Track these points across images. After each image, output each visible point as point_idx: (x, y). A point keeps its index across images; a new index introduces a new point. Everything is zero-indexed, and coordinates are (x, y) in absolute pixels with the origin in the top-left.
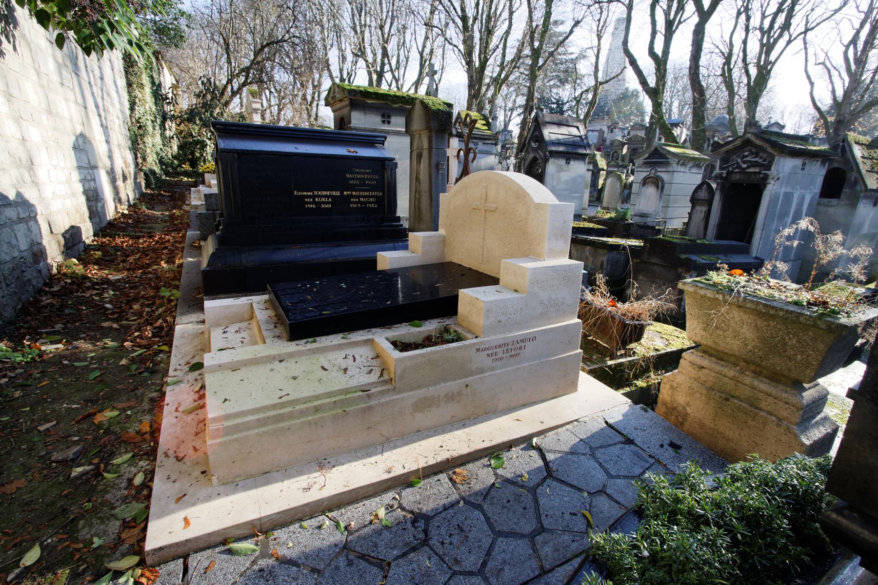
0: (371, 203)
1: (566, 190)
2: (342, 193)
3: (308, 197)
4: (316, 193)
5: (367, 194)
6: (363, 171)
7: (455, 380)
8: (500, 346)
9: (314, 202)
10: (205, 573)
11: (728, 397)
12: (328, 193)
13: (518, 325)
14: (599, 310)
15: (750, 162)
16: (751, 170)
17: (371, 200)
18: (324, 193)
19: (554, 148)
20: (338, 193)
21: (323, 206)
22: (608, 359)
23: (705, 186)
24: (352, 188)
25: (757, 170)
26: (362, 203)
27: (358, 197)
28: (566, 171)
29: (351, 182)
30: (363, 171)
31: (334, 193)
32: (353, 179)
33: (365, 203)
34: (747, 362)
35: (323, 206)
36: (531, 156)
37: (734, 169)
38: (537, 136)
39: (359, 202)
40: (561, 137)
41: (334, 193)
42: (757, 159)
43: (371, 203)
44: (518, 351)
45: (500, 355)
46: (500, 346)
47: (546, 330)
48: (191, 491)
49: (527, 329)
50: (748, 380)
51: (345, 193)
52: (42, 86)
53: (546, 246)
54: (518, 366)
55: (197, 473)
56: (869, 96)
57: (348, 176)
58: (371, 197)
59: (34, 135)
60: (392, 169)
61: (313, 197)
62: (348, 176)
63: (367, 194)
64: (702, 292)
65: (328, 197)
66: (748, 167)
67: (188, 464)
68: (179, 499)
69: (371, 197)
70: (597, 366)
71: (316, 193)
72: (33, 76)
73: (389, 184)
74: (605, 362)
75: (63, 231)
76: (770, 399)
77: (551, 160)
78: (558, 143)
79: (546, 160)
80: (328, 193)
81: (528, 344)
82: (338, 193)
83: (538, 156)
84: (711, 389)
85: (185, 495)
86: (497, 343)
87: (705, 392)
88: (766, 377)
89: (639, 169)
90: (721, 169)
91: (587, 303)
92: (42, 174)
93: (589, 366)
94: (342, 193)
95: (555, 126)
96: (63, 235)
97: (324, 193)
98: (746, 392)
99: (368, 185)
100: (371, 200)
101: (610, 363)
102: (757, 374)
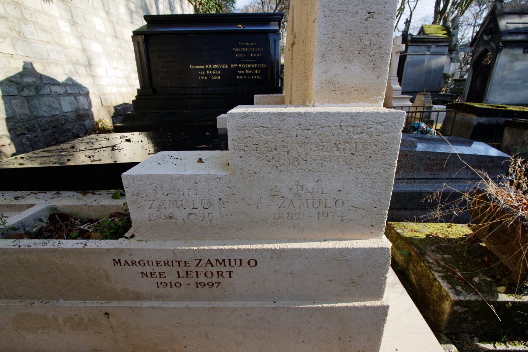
1: (519, 79)
2: (229, 66)
3: (201, 70)
4: (207, 66)
5: (253, 66)
6: (248, 44)
7: (85, 300)
8: (166, 263)
9: (206, 75)
13: (220, 231)
14: (503, 211)
17: (256, 72)
19: (509, 38)
20: (226, 66)
21: (213, 78)
22: (502, 289)
24: (239, 61)
26: (248, 75)
27: (244, 69)
28: (522, 60)
29: (237, 55)
30: (248, 44)
31: (223, 66)
32: (240, 52)
33: (251, 75)
35: (213, 78)
36: (481, 49)
38: (491, 29)
39: (245, 74)
40: (521, 26)
41: (223, 66)
44: (215, 279)
45: (172, 278)
46: (166, 263)
47: (283, 251)
49: (242, 241)
51: (232, 66)
52: (111, 22)
53: (317, 75)
54: (218, 304)
57: (234, 49)
58: (256, 69)
59: (95, 48)
60: (275, 41)
61: (205, 70)
62: (234, 49)
63: (253, 66)
65: (217, 69)
69: (256, 69)
70: (473, 298)
71: (207, 66)
72: (102, 14)
74: (495, 294)
75: (116, 105)
77: (504, 51)
78: (517, 32)
79: (497, 51)
80: (216, 66)
81: (237, 271)
82: (226, 66)
83: (488, 48)
86: (155, 257)
91: (484, 197)
92: (99, 71)
93: (458, 293)
94: (229, 66)
95: (516, 16)
96: (115, 107)
99: (253, 58)
100: (256, 72)
101: (503, 297)
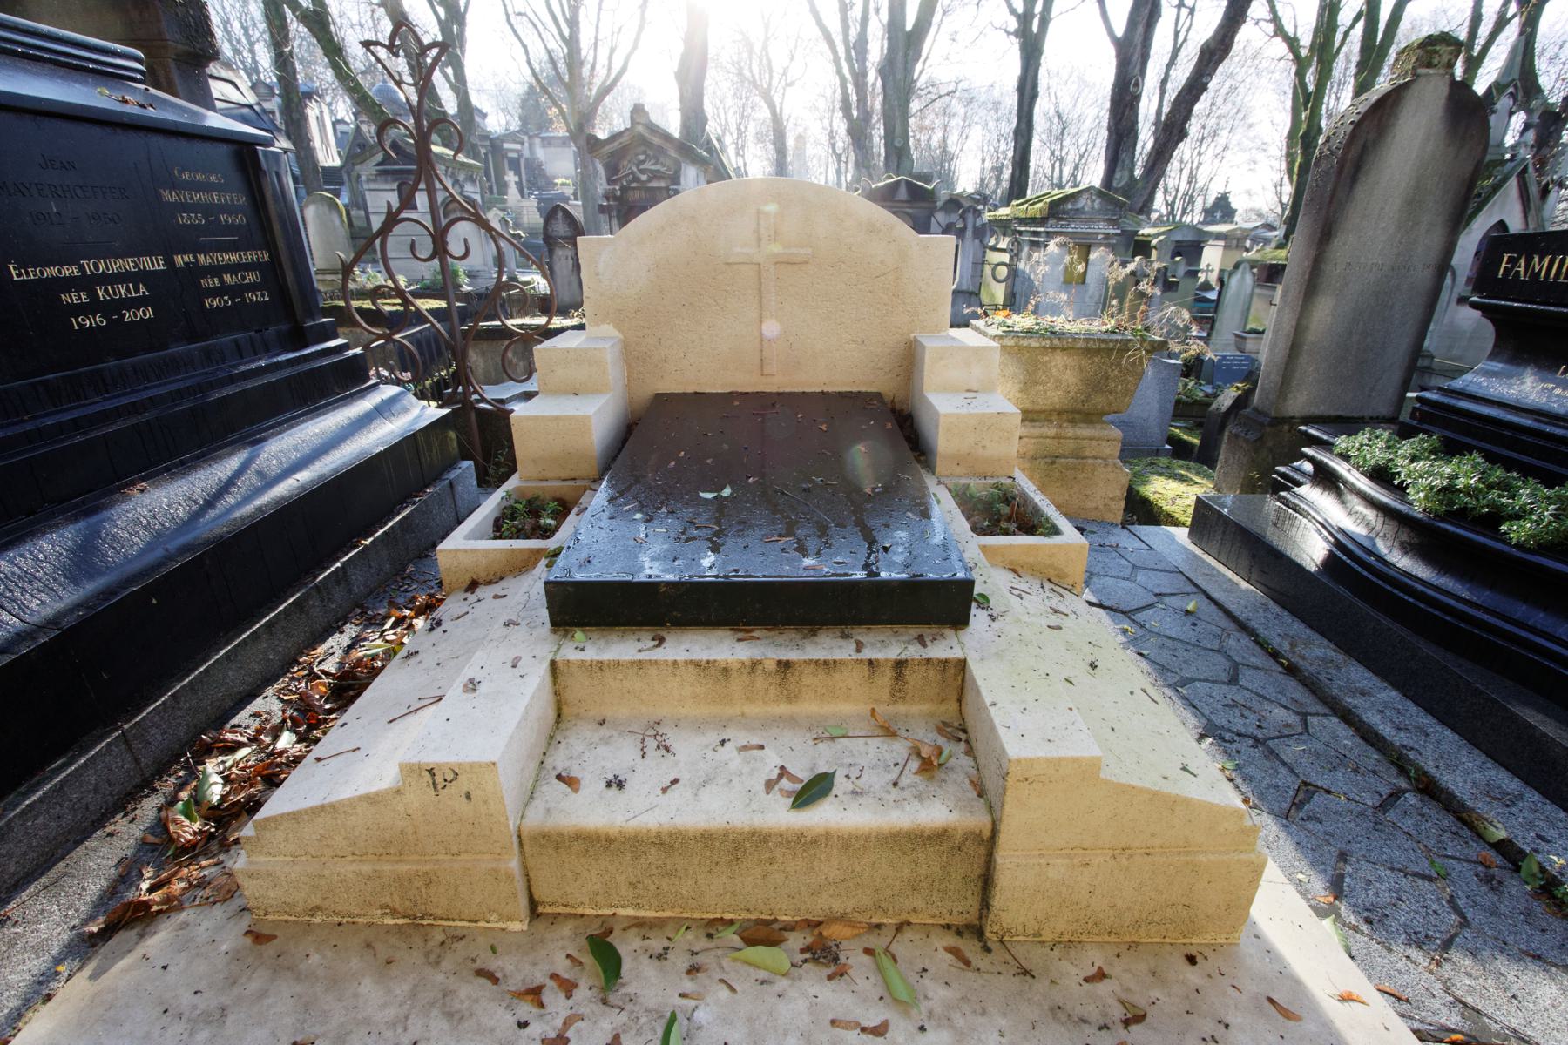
0: (253, 287)
4: (89, 265)
5: (233, 257)
10: (1407, 1001)
11: (1053, 459)
12: (129, 265)
15: (651, 171)
16: (654, 184)
17: (251, 277)
18: (116, 265)
23: (560, 215)
25: (662, 184)
34: (1060, 413)
37: (630, 182)
42: (658, 167)
43: (253, 287)
48: (1250, 987)
50: (1070, 432)
51: (179, 260)
55: (1192, 975)
56: (1329, 117)
63: (233, 257)
64: (1025, 343)
66: (650, 180)
67: (1155, 993)
68: (1286, 1014)
73: (281, 217)
76: (1094, 443)
80: (129, 265)
84: (1034, 458)
85: (1271, 1000)
87: (1027, 465)
88: (1083, 421)
89: (372, 186)
90: (610, 182)
94: (170, 262)
97: (116, 265)
98: (1071, 445)
100: (251, 277)
102: (1073, 422)
